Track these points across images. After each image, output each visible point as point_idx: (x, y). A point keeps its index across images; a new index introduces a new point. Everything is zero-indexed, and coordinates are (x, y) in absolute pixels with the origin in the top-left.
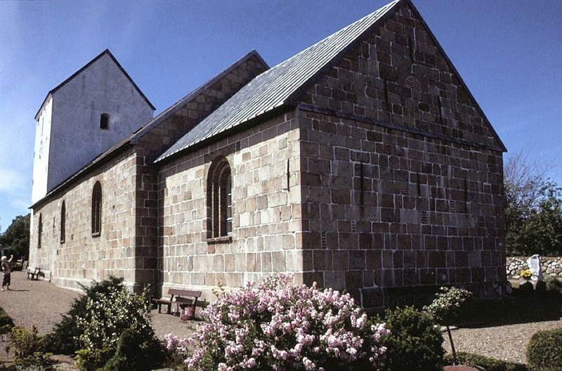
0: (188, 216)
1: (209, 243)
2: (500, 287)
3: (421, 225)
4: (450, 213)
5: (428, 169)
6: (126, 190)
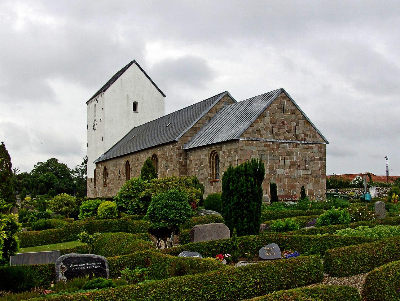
0: (202, 172)
1: (104, 187)
2: (321, 197)
3: (285, 174)
4: (298, 170)
5: (288, 154)
6: (173, 160)
